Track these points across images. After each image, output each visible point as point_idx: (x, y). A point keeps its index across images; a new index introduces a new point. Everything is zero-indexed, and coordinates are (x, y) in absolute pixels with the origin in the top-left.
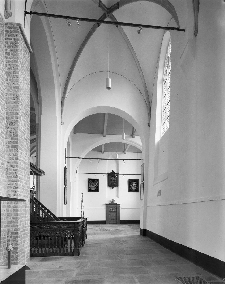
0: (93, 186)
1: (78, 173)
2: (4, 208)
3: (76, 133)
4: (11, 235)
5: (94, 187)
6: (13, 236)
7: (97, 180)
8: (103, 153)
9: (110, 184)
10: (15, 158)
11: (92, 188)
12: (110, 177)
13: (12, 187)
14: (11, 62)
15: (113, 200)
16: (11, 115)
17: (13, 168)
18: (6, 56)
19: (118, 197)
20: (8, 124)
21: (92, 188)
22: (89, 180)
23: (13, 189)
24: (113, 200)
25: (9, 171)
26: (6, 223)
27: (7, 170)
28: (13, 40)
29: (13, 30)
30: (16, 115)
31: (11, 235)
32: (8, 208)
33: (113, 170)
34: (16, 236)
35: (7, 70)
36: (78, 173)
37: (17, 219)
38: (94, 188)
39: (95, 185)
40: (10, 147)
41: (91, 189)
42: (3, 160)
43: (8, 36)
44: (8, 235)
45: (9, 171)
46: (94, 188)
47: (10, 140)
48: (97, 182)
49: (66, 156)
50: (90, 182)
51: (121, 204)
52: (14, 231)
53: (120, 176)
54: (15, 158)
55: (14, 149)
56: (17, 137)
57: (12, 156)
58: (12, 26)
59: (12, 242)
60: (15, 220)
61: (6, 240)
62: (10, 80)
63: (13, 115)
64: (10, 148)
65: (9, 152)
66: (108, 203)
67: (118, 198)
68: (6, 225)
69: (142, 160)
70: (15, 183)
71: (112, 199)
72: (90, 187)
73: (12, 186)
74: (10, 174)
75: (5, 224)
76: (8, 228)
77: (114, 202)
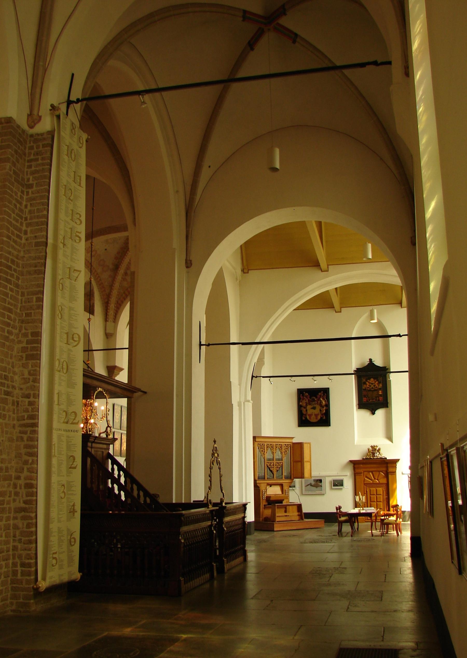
0: (314, 408)
1: (257, 377)
2: (7, 482)
3: (248, 270)
4: (20, 537)
5: (317, 411)
6: (23, 539)
7: (326, 392)
8: (341, 312)
9: (364, 399)
10: (31, 380)
11: (310, 415)
12: (364, 380)
13: (25, 439)
14: (34, 199)
15: (374, 450)
16: (29, 297)
17: (27, 400)
18: (27, 190)
19: (389, 437)
20: (22, 314)
21: (310, 415)
22: (301, 393)
23: (26, 442)
24: (374, 450)
25: (21, 406)
26: (13, 513)
27: (18, 404)
28: (40, 162)
29: (41, 144)
30: (37, 296)
31: (20, 537)
32: (16, 481)
33: (371, 360)
34: (29, 538)
35: (26, 214)
36: (257, 377)
37: (31, 504)
38: (316, 415)
39: (318, 407)
40: (24, 359)
41: (306, 418)
42: (8, 387)
43: (32, 155)
44: (14, 536)
45: (21, 406)
46: (316, 415)
47: (24, 345)
48: (324, 399)
49: (200, 342)
50: (303, 399)
51: (398, 460)
52: (25, 530)
53: (392, 377)
54: (31, 380)
55: (30, 362)
56: (36, 338)
57: (26, 376)
58: (40, 137)
59: (22, 552)
60: (27, 506)
61: (11, 548)
62: (31, 231)
63: (31, 297)
64: (24, 361)
65: (21, 369)
66: (357, 457)
67: (392, 442)
68: (12, 515)
69: (403, 337)
70: (29, 429)
71: (372, 447)
72: (304, 412)
73: (25, 437)
74: (22, 411)
75: (9, 513)
76: (16, 521)
77: (377, 454)
